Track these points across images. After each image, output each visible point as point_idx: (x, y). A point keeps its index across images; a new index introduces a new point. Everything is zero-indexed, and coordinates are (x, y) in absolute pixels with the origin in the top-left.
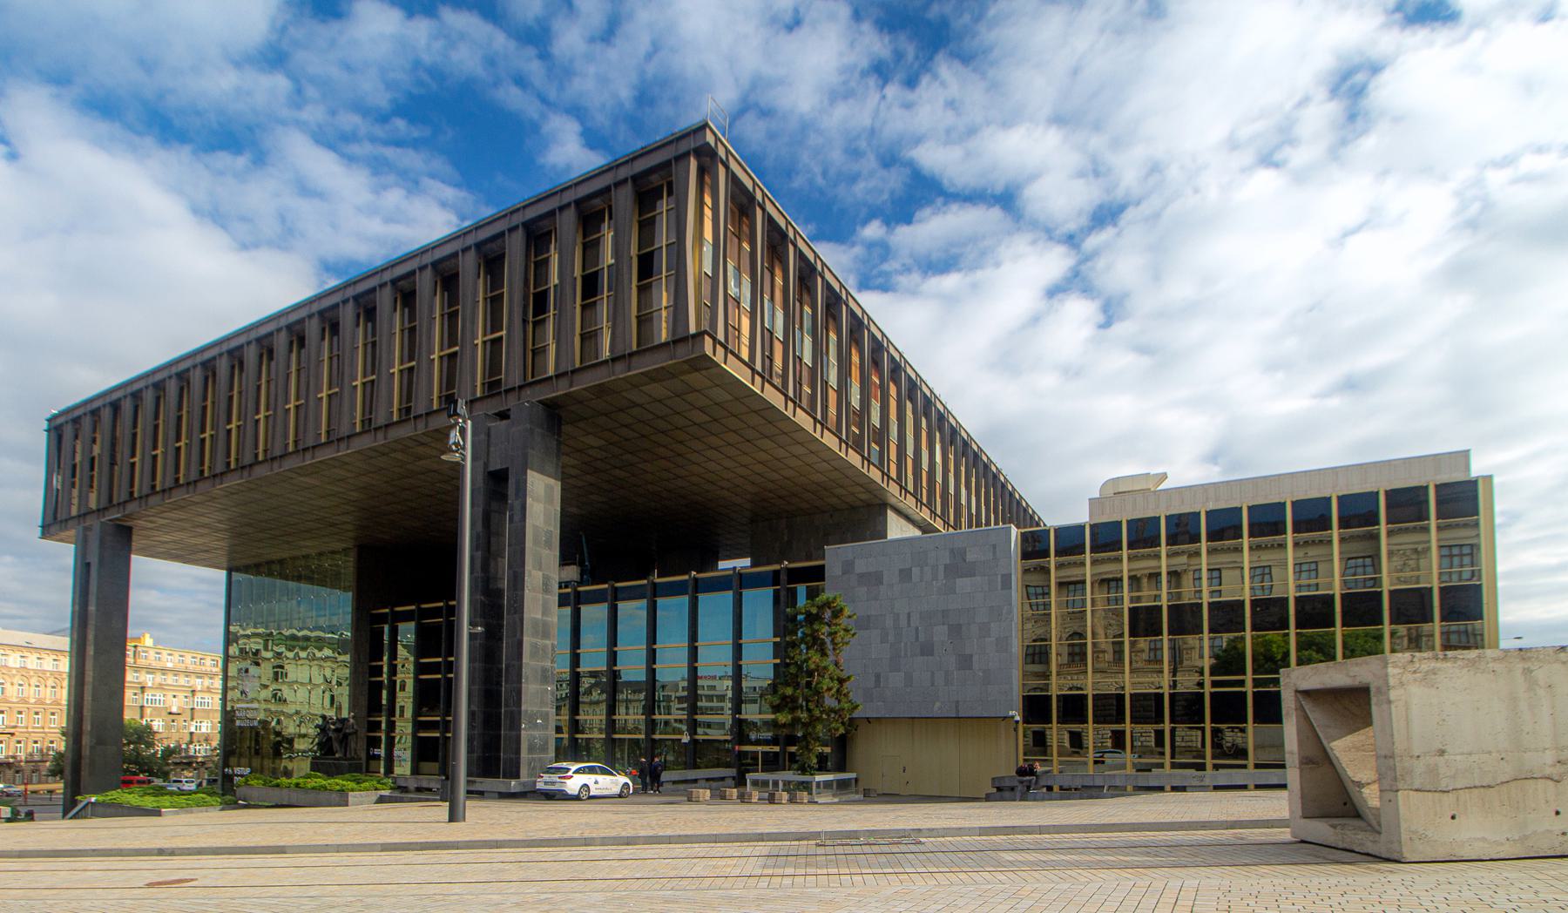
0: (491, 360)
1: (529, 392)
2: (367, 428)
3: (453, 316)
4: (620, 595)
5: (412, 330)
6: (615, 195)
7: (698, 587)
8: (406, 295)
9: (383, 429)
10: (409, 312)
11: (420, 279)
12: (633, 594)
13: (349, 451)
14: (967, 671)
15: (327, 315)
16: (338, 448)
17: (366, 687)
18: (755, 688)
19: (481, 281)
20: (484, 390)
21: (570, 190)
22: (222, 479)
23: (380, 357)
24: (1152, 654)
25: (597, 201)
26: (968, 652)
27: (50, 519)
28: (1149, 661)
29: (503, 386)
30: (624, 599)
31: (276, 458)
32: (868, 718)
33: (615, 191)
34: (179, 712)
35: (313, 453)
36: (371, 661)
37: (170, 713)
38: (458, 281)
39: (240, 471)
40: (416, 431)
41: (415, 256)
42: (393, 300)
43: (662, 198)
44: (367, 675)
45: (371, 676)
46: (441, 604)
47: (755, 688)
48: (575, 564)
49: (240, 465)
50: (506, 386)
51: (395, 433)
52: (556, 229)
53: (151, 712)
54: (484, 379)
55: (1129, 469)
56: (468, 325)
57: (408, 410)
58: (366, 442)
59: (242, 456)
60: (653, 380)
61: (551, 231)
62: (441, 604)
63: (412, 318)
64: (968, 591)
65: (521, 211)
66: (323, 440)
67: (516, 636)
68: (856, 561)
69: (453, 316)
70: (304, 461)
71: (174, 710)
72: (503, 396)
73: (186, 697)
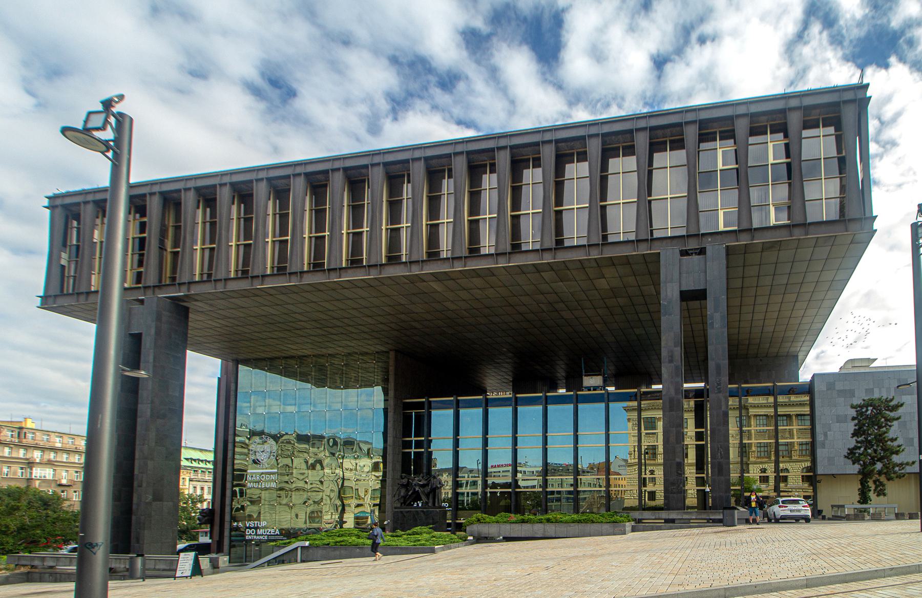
0: (315, 250)
1: (710, 240)
2: (205, 278)
3: (248, 221)
4: (519, 402)
5: (213, 224)
6: (332, 176)
7: (547, 401)
8: (280, 192)
9: (152, 288)
10: (211, 211)
11: (185, 197)
12: (444, 406)
13: (55, 305)
14: (911, 447)
15: (274, 182)
16: (290, 280)
17: (400, 457)
18: (533, 472)
19: (308, 198)
20: (348, 263)
21: (379, 156)
22: (263, 281)
23: (220, 234)
24: (759, 454)
25: (484, 157)
26: (911, 437)
27: (55, 290)
28: (758, 457)
29: (177, 280)
30: (522, 405)
31: (149, 287)
32: (833, 475)
33: (332, 174)
34: (69, 484)
35: (509, 258)
36: (404, 437)
37: (61, 485)
38: (181, 207)
39: (76, 296)
40: (189, 291)
41: (147, 185)
42: (197, 201)
43: (487, 174)
44: (401, 448)
45: (404, 448)
46: (424, 400)
47: (533, 472)
48: (601, 375)
49: (76, 291)
50: (215, 277)
51: (232, 286)
52: (368, 179)
53: (40, 483)
54: (348, 257)
55: (858, 353)
56: (260, 228)
57: (209, 275)
58: (309, 279)
59: (180, 274)
60: (479, 276)
61: (404, 176)
62: (424, 400)
63: (213, 215)
64: (910, 403)
65: (371, 156)
66: (197, 278)
67: (720, 408)
68: (836, 383)
69: (248, 221)
70: (380, 273)
71: (64, 482)
72: (299, 276)
73: (77, 472)
